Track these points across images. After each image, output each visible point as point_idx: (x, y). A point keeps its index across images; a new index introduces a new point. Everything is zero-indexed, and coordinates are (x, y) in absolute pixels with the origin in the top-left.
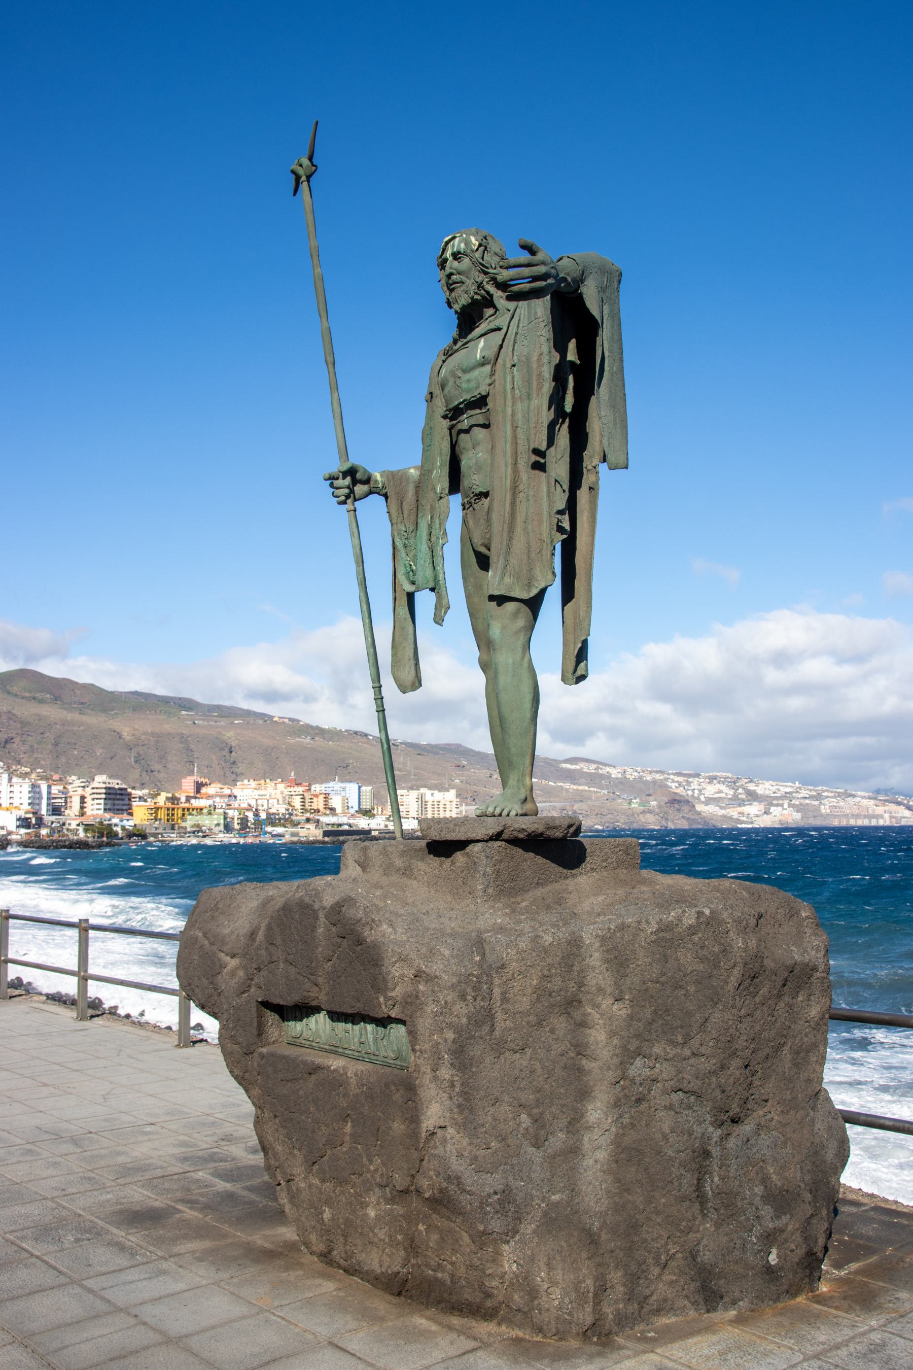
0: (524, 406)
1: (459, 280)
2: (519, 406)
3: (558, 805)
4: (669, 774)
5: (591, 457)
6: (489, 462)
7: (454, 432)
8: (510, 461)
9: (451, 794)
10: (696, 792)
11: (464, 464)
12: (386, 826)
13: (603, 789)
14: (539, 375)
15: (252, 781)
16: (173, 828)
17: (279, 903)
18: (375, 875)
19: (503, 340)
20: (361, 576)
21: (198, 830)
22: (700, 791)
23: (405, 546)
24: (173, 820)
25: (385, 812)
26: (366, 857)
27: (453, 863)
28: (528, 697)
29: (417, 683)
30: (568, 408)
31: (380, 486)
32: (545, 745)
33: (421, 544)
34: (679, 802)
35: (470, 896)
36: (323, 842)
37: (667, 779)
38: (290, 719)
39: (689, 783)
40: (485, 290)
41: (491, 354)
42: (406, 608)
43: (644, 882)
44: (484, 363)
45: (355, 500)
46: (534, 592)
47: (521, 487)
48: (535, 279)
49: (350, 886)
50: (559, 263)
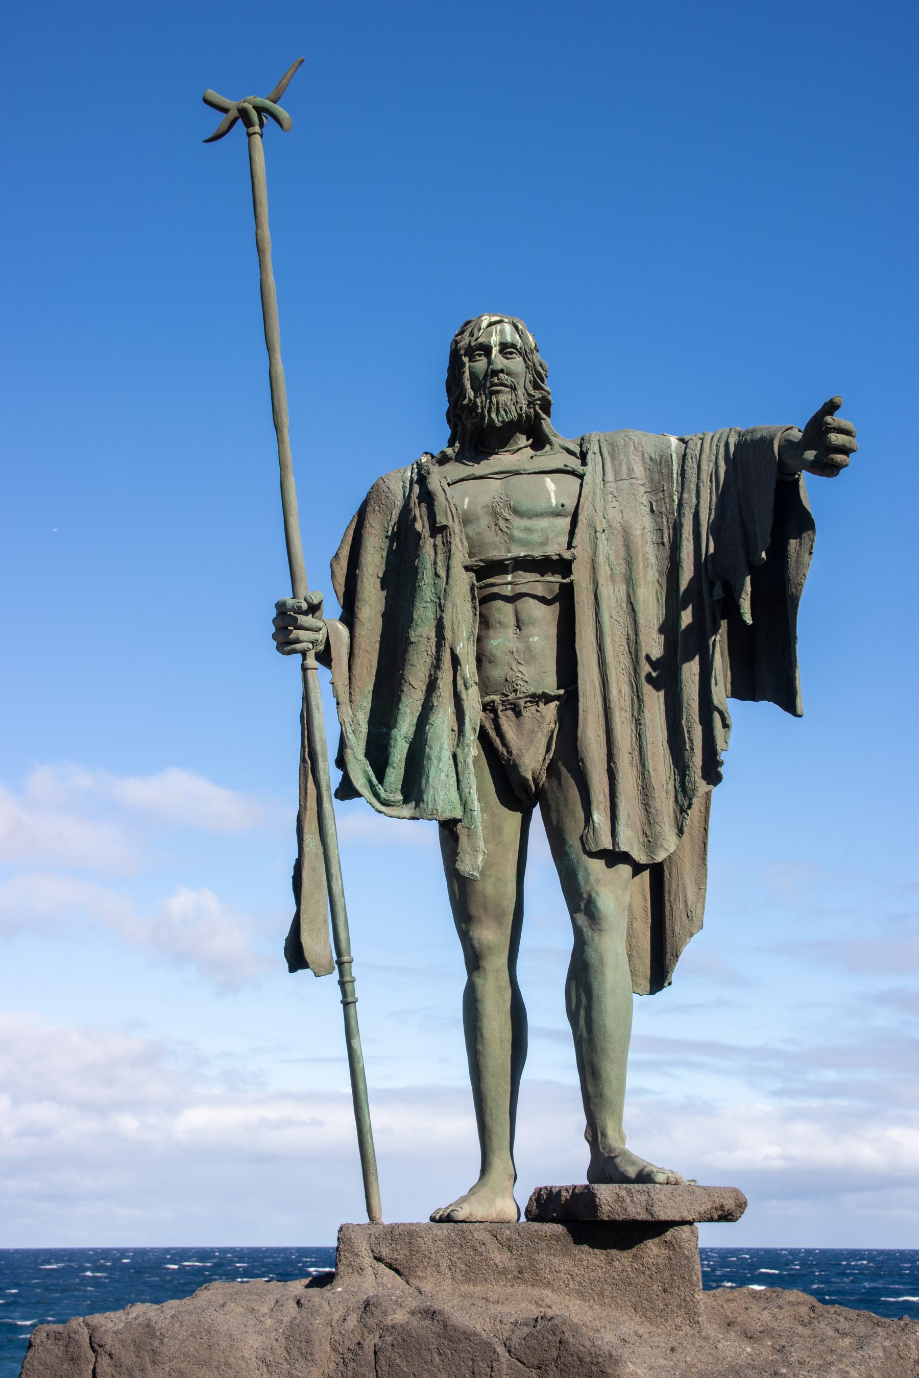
1: (509, 383)
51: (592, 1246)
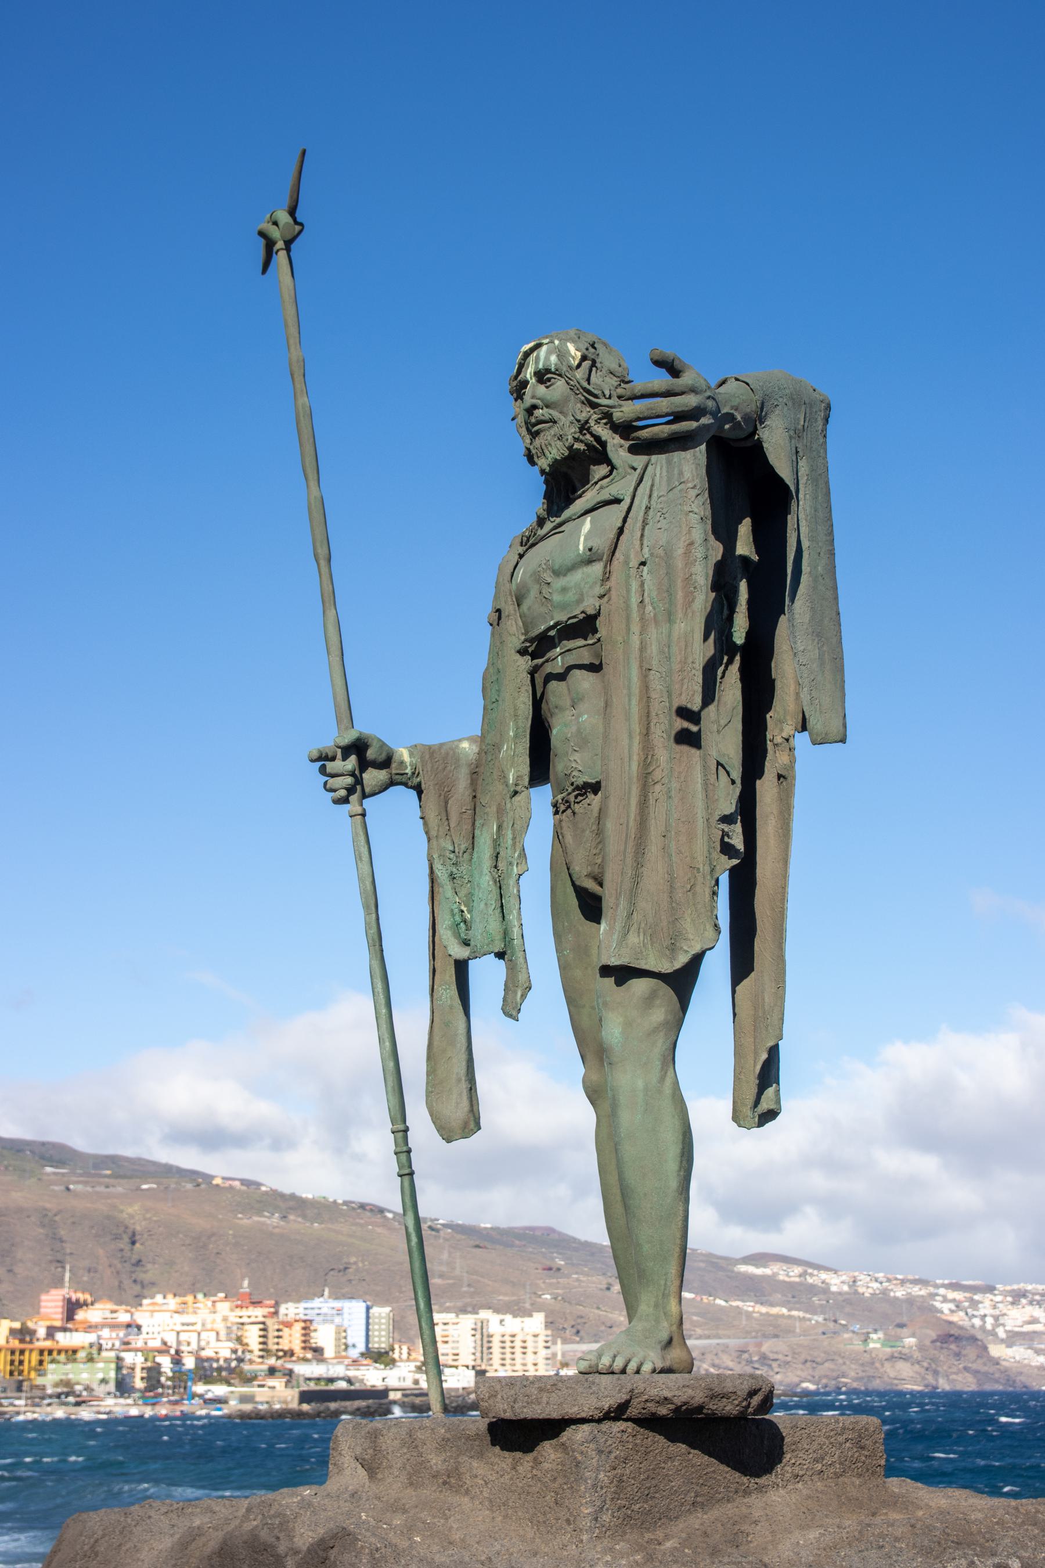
0: (662, 635)
1: (547, 417)
2: (653, 633)
3: (734, 1343)
4: (937, 1286)
5: (781, 722)
6: (601, 729)
7: (539, 679)
8: (636, 728)
9: (536, 1322)
10: (989, 1321)
11: (557, 732)
12: (416, 1382)
13: (814, 1313)
14: (688, 579)
15: (170, 1296)
16: (19, 1388)
17: (213, 1541)
18: (393, 1485)
19: (625, 520)
20: (374, 930)
21: (66, 1392)
22: (996, 1318)
23: (452, 877)
24: (21, 1373)
25: (414, 1355)
26: (377, 1450)
27: (537, 1462)
28: (673, 1151)
29: (472, 1123)
30: (739, 637)
31: (408, 771)
32: (707, 1229)
33: (481, 874)
34: (958, 1339)
35: (569, 1529)
36: (300, 1415)
37: (933, 1296)
38: (243, 1182)
39: (975, 1304)
40: (593, 435)
41: (603, 543)
42: (454, 987)
43: (894, 1502)
44: (591, 558)
45: (364, 796)
46: (682, 960)
47: (657, 775)
48: (679, 417)
49: (346, 1507)
50: (722, 390)
51: (502, 1449)
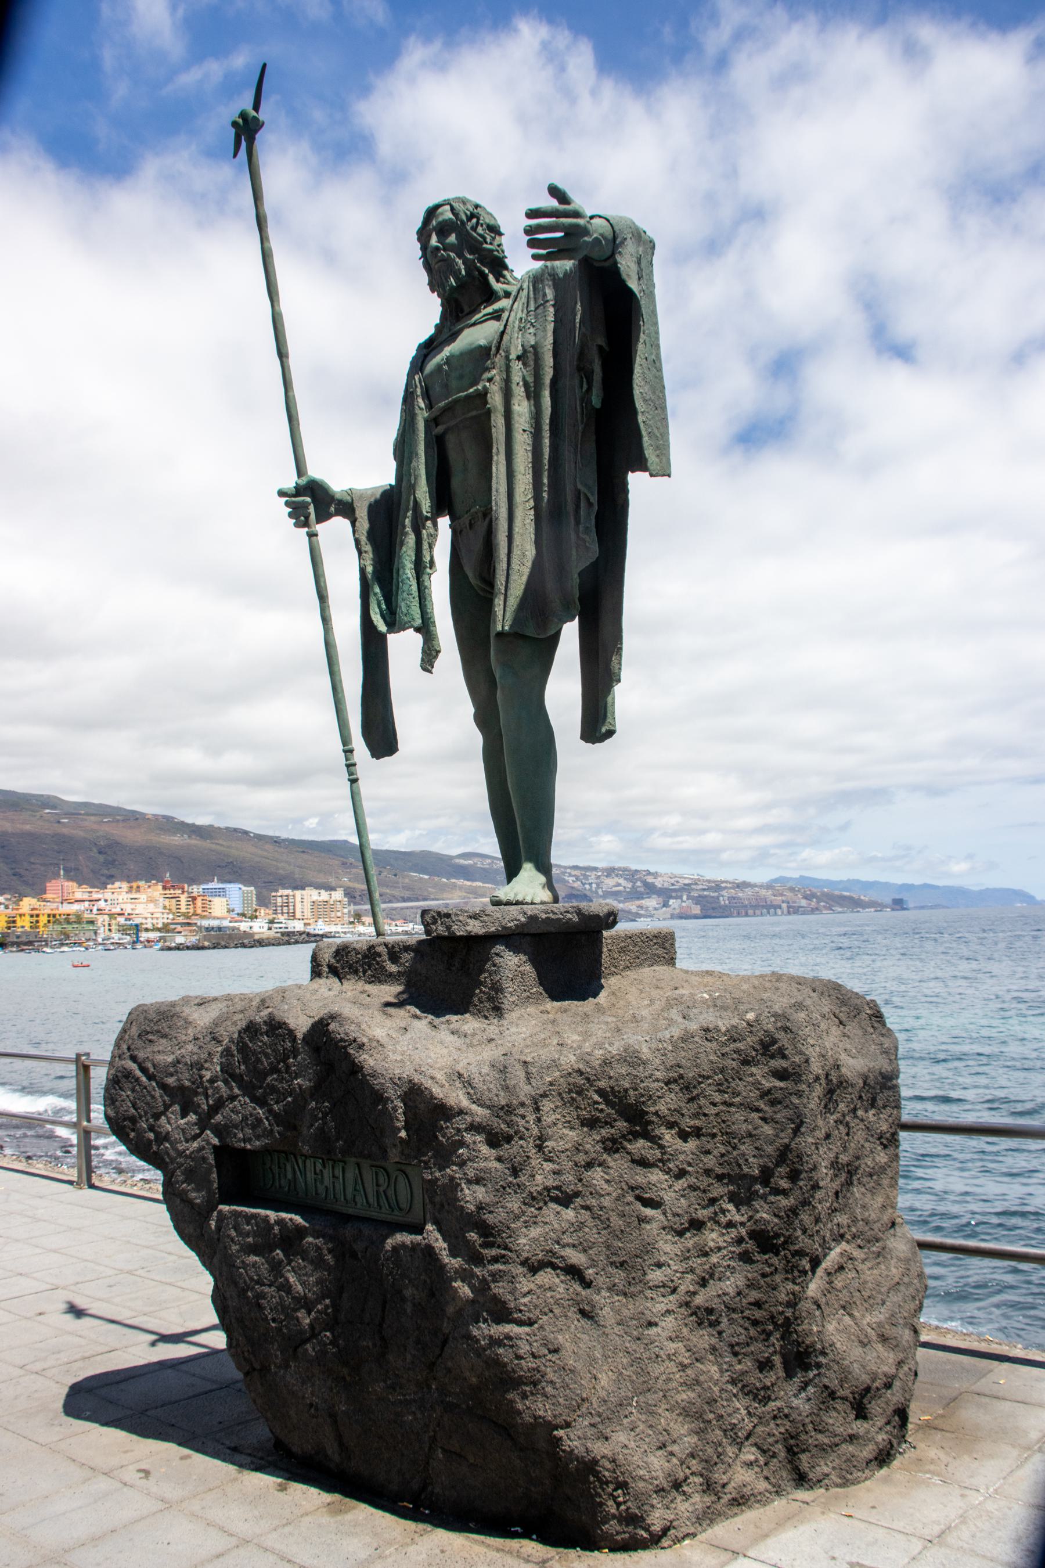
9: (338, 895)
10: (594, 886)
22: (598, 885)
